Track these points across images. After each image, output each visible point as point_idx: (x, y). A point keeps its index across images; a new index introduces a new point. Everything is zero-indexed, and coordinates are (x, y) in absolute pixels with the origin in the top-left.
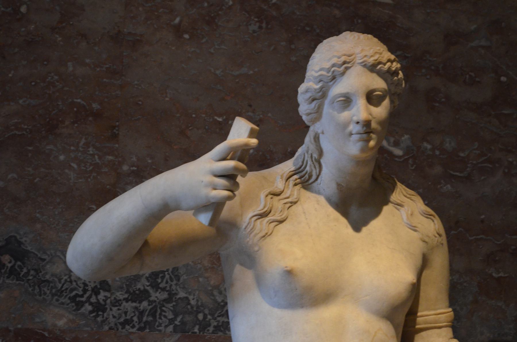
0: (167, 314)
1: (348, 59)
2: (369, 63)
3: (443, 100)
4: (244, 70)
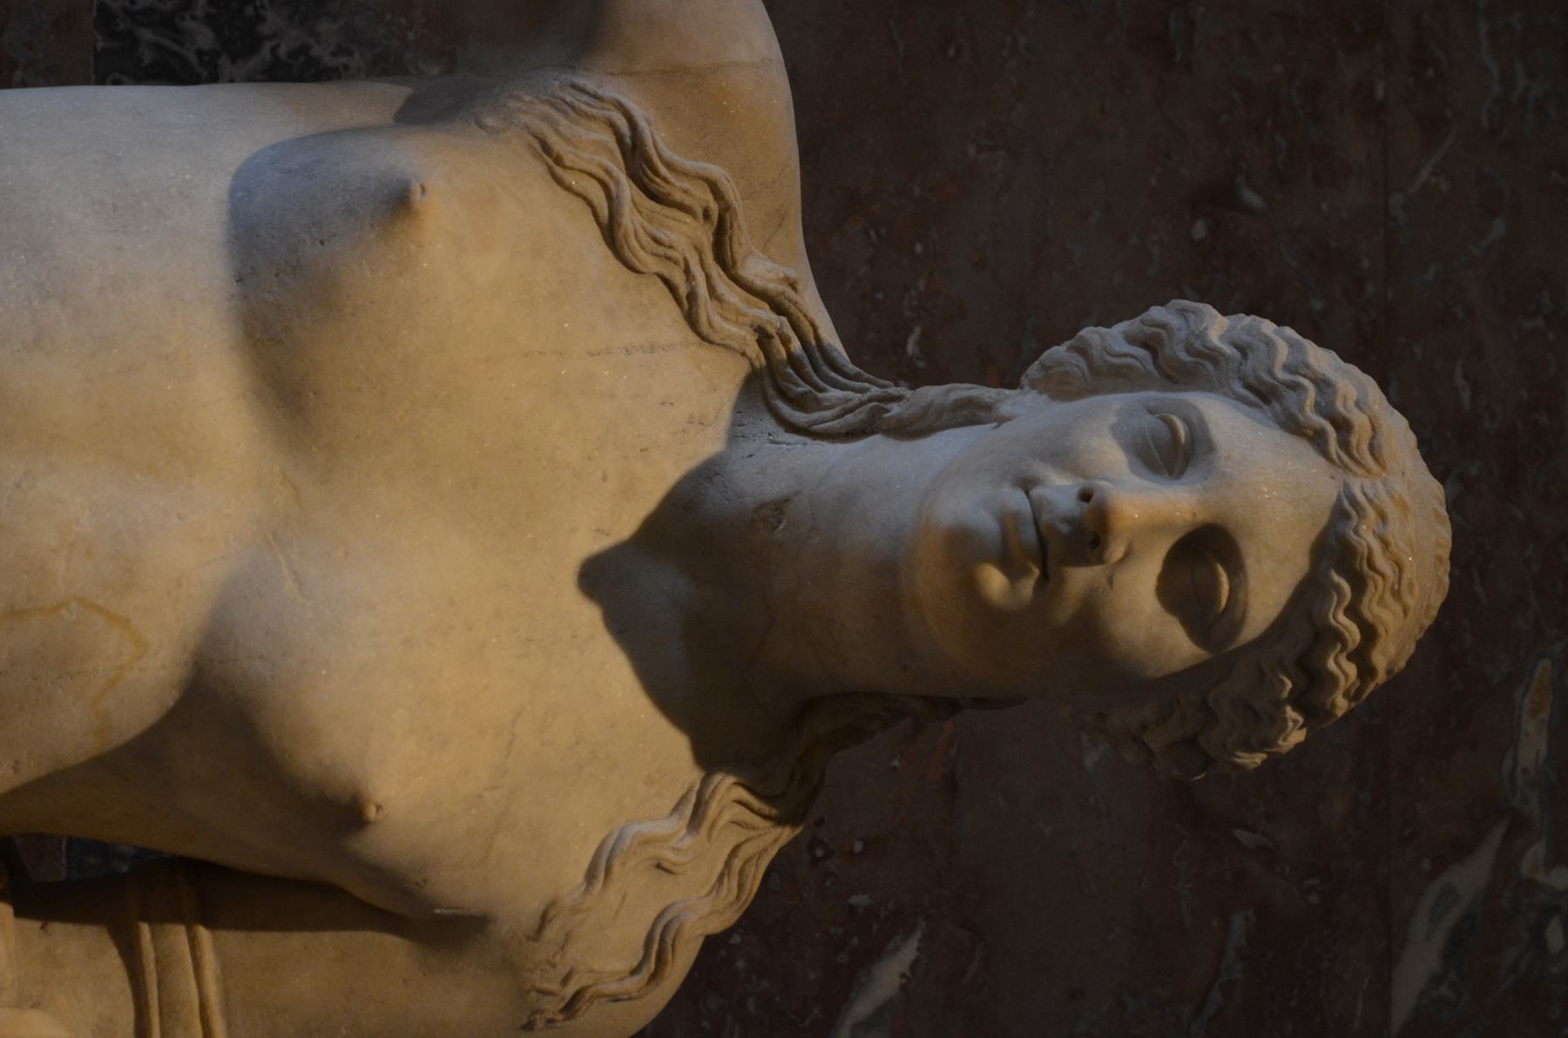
1: (1359, 440)
2: (1356, 531)
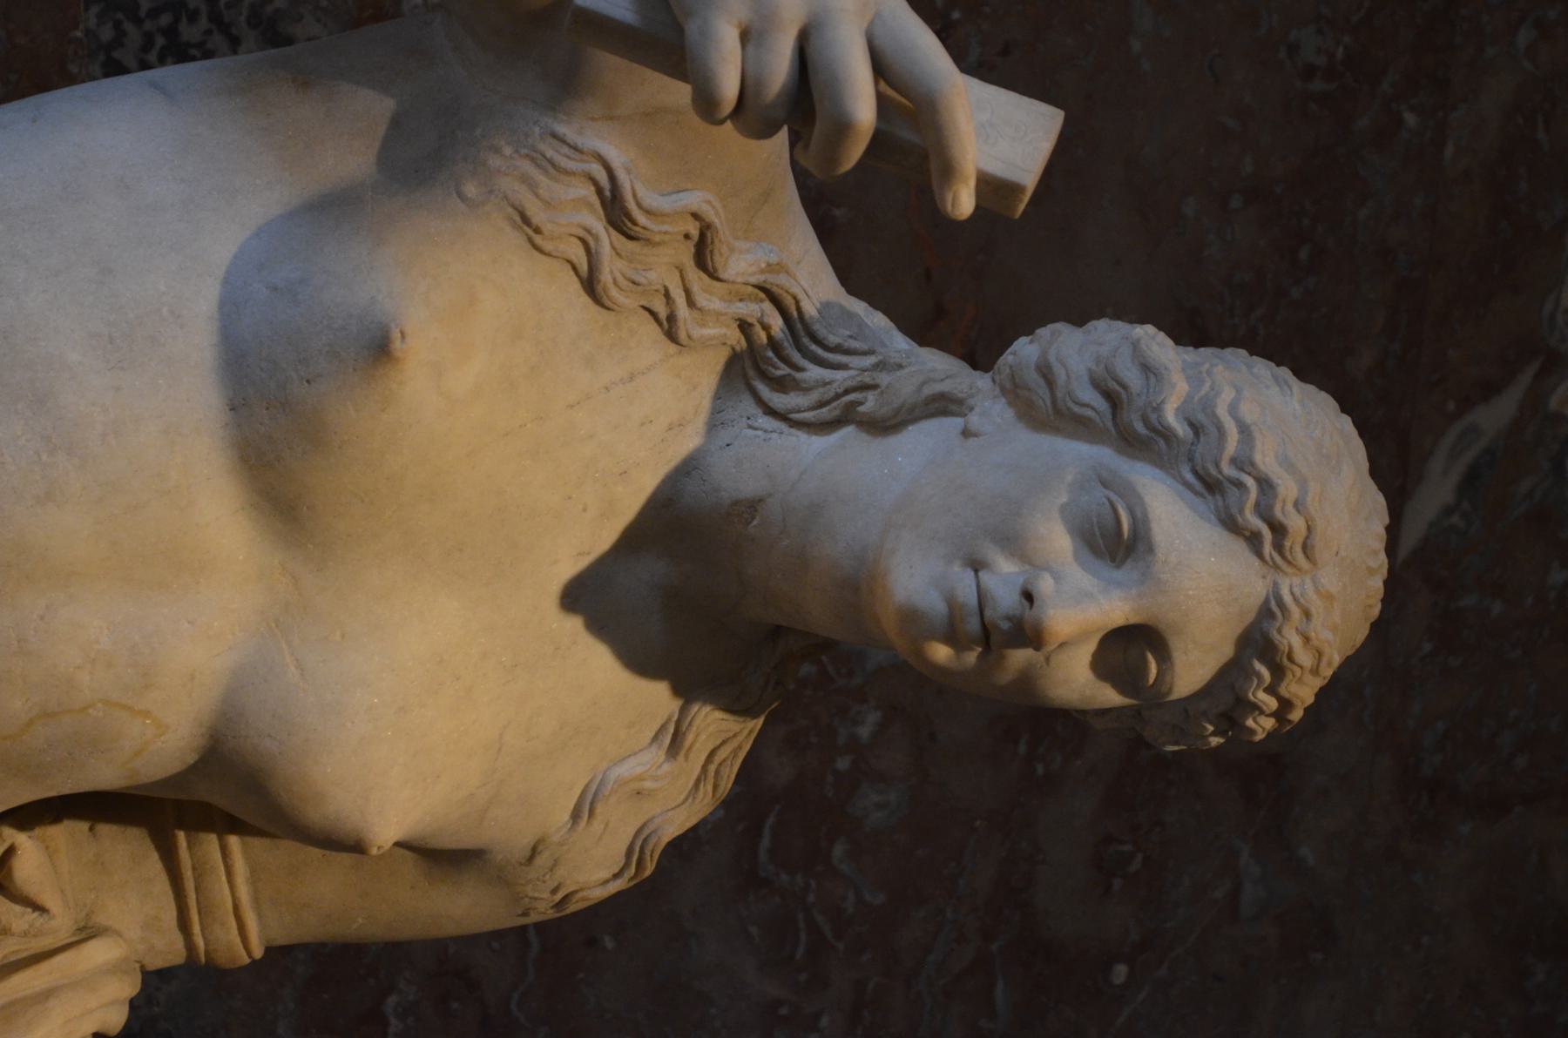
2: (1279, 631)
3: (1040, 769)
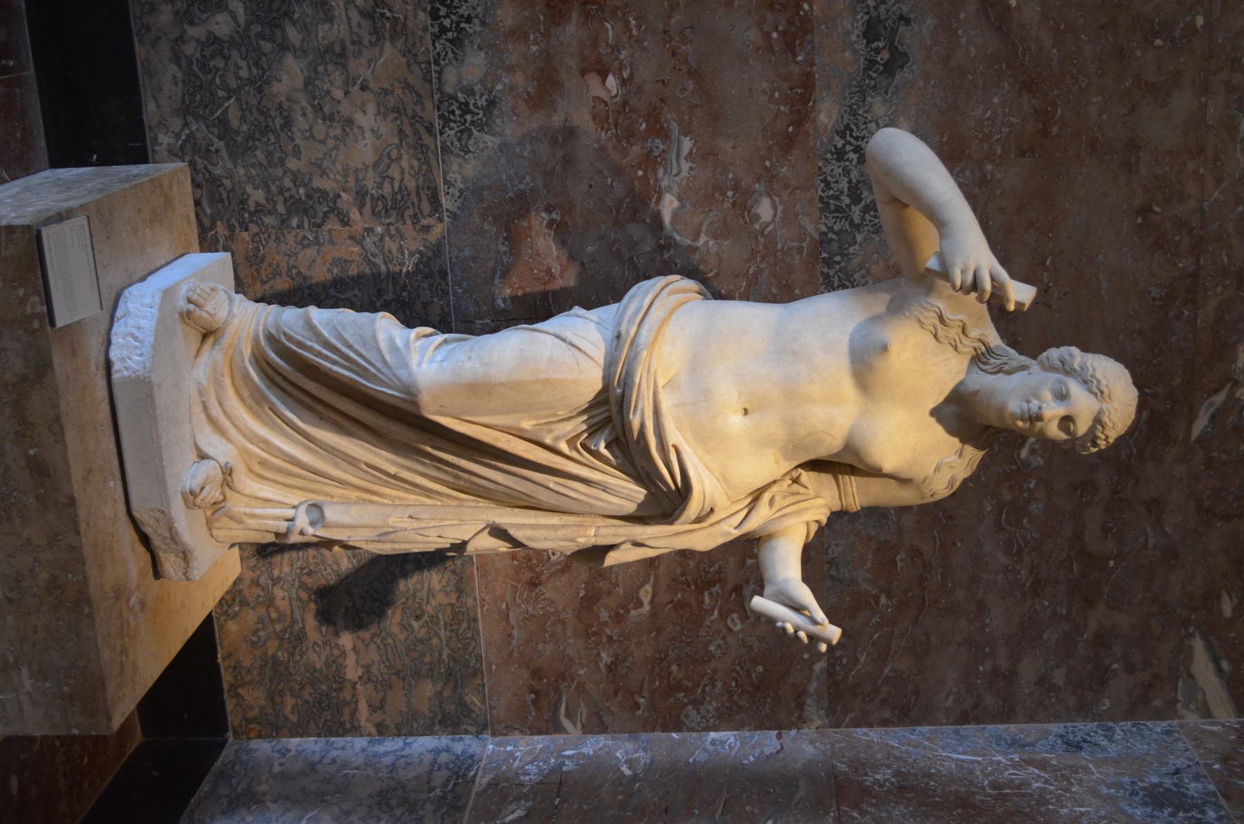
0: (838, 223)
3: (1084, 500)
4: (1105, 285)
